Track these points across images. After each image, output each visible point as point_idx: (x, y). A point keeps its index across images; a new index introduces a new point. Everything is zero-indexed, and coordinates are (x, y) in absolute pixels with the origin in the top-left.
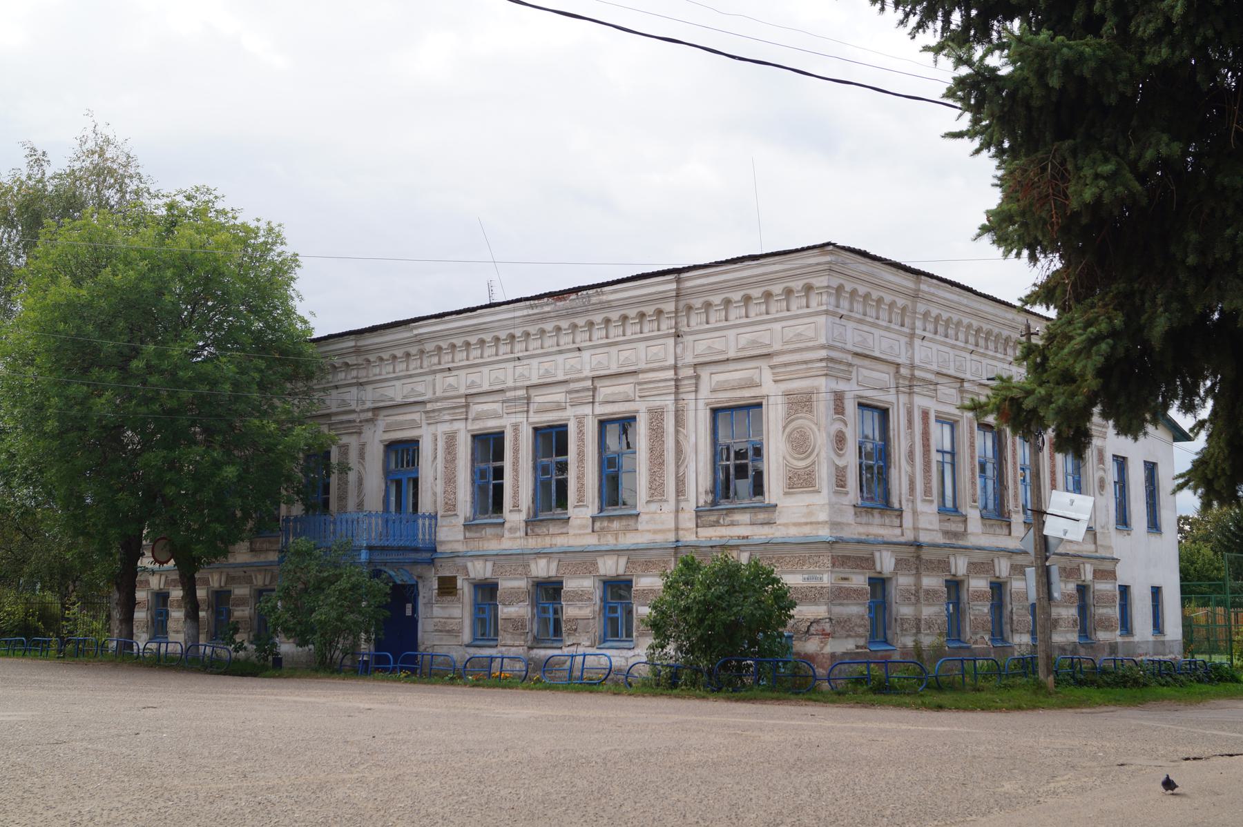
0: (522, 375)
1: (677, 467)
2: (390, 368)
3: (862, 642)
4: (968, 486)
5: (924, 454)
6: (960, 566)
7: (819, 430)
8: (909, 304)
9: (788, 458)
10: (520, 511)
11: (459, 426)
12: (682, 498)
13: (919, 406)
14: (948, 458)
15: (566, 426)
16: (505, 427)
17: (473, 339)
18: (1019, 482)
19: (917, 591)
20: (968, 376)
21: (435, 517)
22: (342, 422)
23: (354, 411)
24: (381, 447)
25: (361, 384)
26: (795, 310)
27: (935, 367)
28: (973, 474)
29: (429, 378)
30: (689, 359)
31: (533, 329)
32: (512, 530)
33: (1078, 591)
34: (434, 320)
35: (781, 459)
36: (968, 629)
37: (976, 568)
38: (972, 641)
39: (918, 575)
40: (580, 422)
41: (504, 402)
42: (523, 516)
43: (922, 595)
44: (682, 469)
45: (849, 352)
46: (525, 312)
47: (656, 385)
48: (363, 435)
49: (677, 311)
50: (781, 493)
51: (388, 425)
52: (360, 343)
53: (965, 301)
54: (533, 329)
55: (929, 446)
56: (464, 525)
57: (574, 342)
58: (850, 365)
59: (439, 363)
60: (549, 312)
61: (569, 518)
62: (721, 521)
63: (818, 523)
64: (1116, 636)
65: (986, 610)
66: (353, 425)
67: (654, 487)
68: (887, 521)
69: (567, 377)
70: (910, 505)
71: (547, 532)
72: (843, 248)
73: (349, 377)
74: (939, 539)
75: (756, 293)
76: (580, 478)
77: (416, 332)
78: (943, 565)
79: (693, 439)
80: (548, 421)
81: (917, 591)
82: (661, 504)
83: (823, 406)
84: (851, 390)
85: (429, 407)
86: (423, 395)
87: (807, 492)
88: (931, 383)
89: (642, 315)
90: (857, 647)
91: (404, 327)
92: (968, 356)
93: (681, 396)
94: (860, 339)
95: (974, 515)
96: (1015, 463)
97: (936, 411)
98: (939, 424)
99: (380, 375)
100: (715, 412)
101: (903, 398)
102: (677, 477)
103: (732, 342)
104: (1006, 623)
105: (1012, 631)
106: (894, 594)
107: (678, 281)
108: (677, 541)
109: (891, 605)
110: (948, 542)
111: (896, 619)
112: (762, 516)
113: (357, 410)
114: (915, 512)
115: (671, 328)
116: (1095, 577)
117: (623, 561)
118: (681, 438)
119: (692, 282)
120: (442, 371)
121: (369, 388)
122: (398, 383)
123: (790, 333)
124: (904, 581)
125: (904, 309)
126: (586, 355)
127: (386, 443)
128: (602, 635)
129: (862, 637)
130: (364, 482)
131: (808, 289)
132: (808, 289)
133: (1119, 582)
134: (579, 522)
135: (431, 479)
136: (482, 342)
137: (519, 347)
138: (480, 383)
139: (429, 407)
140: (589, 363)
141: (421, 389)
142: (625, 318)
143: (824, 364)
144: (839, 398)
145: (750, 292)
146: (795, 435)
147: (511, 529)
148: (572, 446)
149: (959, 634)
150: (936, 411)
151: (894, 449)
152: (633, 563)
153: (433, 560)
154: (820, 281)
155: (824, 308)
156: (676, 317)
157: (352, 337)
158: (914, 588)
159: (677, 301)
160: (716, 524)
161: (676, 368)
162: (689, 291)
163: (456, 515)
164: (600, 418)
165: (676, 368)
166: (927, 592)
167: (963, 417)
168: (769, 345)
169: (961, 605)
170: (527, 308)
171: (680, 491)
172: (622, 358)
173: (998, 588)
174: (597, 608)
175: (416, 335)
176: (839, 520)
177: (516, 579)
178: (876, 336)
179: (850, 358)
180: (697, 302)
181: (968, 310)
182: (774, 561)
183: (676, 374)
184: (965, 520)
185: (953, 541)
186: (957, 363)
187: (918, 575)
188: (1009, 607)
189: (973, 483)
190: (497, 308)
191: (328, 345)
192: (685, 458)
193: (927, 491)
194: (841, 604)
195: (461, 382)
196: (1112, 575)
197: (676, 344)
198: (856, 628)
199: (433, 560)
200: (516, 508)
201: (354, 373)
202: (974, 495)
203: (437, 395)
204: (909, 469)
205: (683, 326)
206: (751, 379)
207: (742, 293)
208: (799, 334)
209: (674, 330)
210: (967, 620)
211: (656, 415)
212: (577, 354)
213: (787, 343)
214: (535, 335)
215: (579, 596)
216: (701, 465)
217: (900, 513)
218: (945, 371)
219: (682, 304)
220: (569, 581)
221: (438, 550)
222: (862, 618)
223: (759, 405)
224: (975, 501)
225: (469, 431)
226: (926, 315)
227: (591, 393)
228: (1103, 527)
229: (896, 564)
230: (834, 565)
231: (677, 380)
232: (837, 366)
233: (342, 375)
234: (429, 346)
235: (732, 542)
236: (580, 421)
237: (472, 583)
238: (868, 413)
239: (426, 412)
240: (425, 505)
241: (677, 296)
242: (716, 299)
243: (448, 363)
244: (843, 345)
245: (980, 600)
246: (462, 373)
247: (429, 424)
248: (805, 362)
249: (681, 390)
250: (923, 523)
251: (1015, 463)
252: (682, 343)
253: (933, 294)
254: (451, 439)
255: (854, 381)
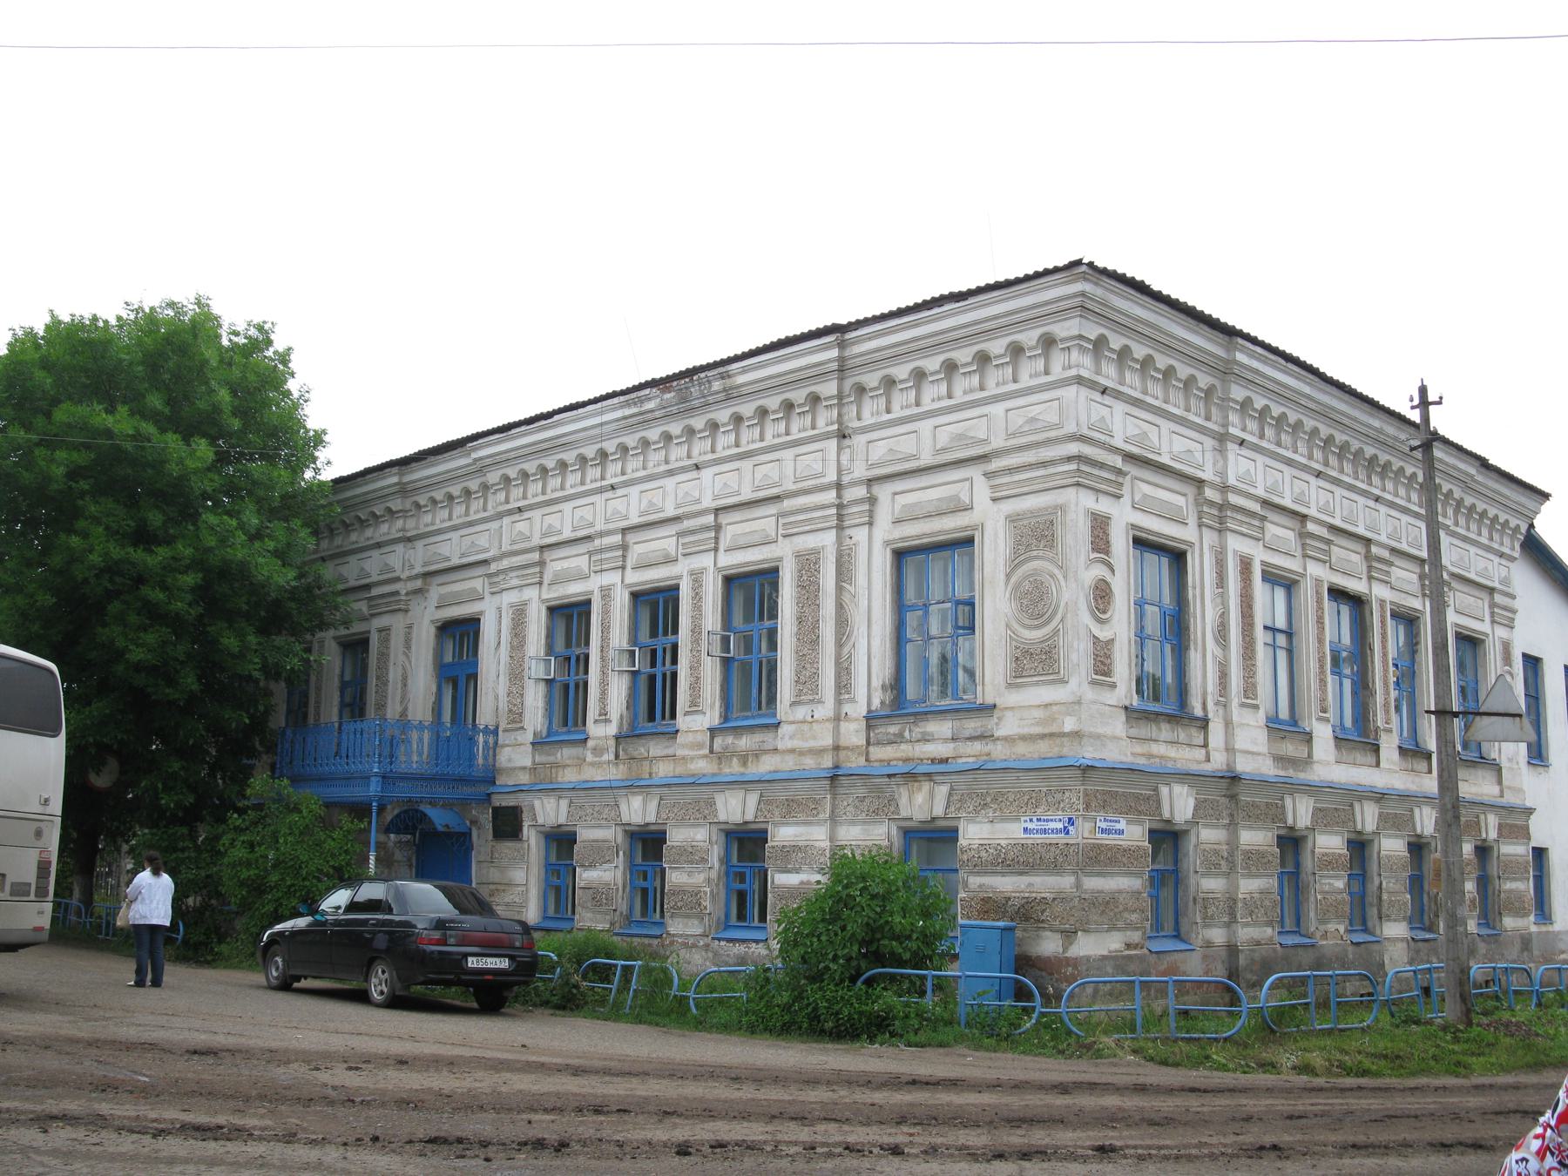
0: (616, 512)
1: (839, 645)
2: (445, 514)
3: (1136, 937)
4: (1314, 685)
5: (1244, 630)
6: (1301, 812)
7: (1065, 577)
8: (1217, 383)
9: (1016, 626)
10: (608, 721)
11: (531, 593)
12: (847, 696)
13: (1235, 552)
14: (1281, 640)
15: (676, 588)
16: (592, 593)
17: (550, 463)
18: (1392, 686)
19: (1231, 854)
20: (1313, 512)
21: (495, 732)
22: (382, 596)
23: (398, 579)
24: (433, 630)
25: (409, 540)
26: (1025, 381)
27: (1260, 492)
28: (1322, 667)
29: (494, 525)
30: (860, 471)
31: (631, 440)
32: (597, 751)
33: (1410, 851)
34: (497, 436)
35: (1002, 628)
36: (1312, 914)
37: (1323, 818)
38: (1318, 934)
39: (1232, 827)
40: (695, 581)
41: (590, 553)
42: (612, 729)
43: (1239, 859)
44: (846, 650)
45: (1115, 450)
46: (619, 414)
47: (809, 516)
48: (410, 614)
49: (840, 396)
50: (1003, 684)
51: (441, 597)
52: (407, 479)
53: (1307, 390)
54: (631, 440)
55: (1251, 616)
56: (533, 744)
57: (689, 457)
58: (1119, 472)
59: (507, 502)
60: (652, 411)
61: (677, 731)
62: (907, 734)
63: (1062, 735)
64: (1529, 923)
65: (1340, 884)
66: (397, 598)
67: (803, 679)
68: (1182, 736)
69: (680, 511)
70: (1221, 712)
71: (646, 755)
72: (1104, 272)
73: (393, 531)
74: (1268, 769)
75: (963, 355)
76: (695, 667)
77: (474, 455)
78: (1274, 813)
79: (863, 603)
80: (652, 581)
81: (1231, 854)
82: (813, 707)
83: (1076, 534)
84: (1123, 517)
85: (494, 567)
86: (486, 550)
87: (1044, 683)
88: (1252, 514)
89: (789, 406)
90: (1128, 946)
91: (459, 450)
92: (1312, 480)
93: (848, 532)
94: (1137, 432)
95: (1323, 734)
96: (1385, 655)
97: (1263, 563)
98: (1268, 586)
99: (433, 524)
100: (900, 555)
101: (1210, 537)
102: (838, 663)
103: (924, 441)
104: (1371, 905)
105: (1380, 918)
106: (1192, 859)
107: (842, 345)
108: (837, 767)
109: (1187, 877)
110: (1282, 773)
111: (1195, 899)
112: (972, 725)
113: (403, 576)
114: (1228, 724)
115: (832, 424)
116: (1500, 834)
117: (753, 799)
118: (846, 598)
119: (864, 345)
120: (510, 512)
121: (419, 544)
122: (455, 535)
123: (1017, 420)
124: (1210, 835)
125: (1209, 392)
126: (707, 474)
127: (439, 624)
128: (723, 917)
129: (1137, 929)
130: (409, 682)
131: (1048, 342)
132: (1048, 342)
133: (1534, 844)
134: (690, 738)
135: (493, 675)
136: (563, 465)
137: (613, 468)
138: (559, 528)
139: (494, 567)
140: (709, 488)
141: (484, 542)
142: (763, 412)
143: (1073, 466)
144: (1100, 525)
145: (954, 355)
146: (1027, 585)
147: (595, 749)
148: (684, 618)
149: (1298, 924)
150: (1263, 563)
151: (1195, 617)
152: (769, 802)
153: (489, 795)
154: (1065, 329)
155: (1073, 372)
156: (840, 405)
157: (395, 470)
158: (1225, 847)
159: (841, 379)
160: (898, 739)
161: (839, 486)
162: (858, 361)
163: (522, 728)
164: (724, 573)
165: (839, 486)
166: (1248, 855)
167: (1305, 575)
168: (985, 441)
169: (1303, 876)
170: (622, 407)
171: (843, 686)
172: (758, 476)
173: (1359, 847)
174: (714, 874)
175: (476, 460)
176: (1100, 730)
177: (600, 826)
178: (1164, 431)
179: (1118, 462)
180: (872, 379)
181: (1313, 406)
182: (989, 799)
183: (839, 496)
184: (1308, 738)
185: (1291, 772)
186: (1297, 490)
187: (1232, 827)
188: (1376, 882)
189: (1323, 682)
190: (581, 411)
191: (366, 484)
192: (851, 632)
193: (1250, 689)
194: (1099, 874)
195: (534, 527)
196: (1523, 833)
197: (840, 449)
198: (1126, 915)
199: (489, 795)
200: (604, 717)
201: (399, 523)
202: (1323, 700)
203: (503, 549)
204: (1219, 652)
205: (851, 420)
206: (956, 498)
207: (942, 358)
208: (1033, 420)
209: (835, 427)
210: (1312, 899)
211: (808, 563)
212: (694, 474)
213: (1013, 435)
214: (635, 448)
215: (691, 855)
216: (876, 643)
217: (1204, 723)
218: (1277, 500)
219: (848, 384)
220: (675, 830)
221: (497, 783)
222: (1136, 894)
223: (969, 541)
224: (1324, 711)
225: (543, 601)
226: (1246, 404)
227: (713, 534)
228: (1510, 760)
229: (1196, 809)
230: (1087, 807)
231: (840, 506)
232: (1096, 472)
233: (384, 528)
234: (493, 477)
235: (921, 769)
236: (697, 577)
237: (541, 832)
238: (1151, 558)
239: (490, 576)
240: (485, 717)
241: (841, 370)
242: (901, 372)
243: (518, 500)
244: (1108, 439)
245: (1333, 869)
246: (536, 514)
247: (493, 593)
248: (1044, 464)
249: (847, 523)
250: (1242, 741)
251: (1385, 655)
252: (849, 447)
253: (1257, 372)
254: (520, 612)
255: (1126, 500)
